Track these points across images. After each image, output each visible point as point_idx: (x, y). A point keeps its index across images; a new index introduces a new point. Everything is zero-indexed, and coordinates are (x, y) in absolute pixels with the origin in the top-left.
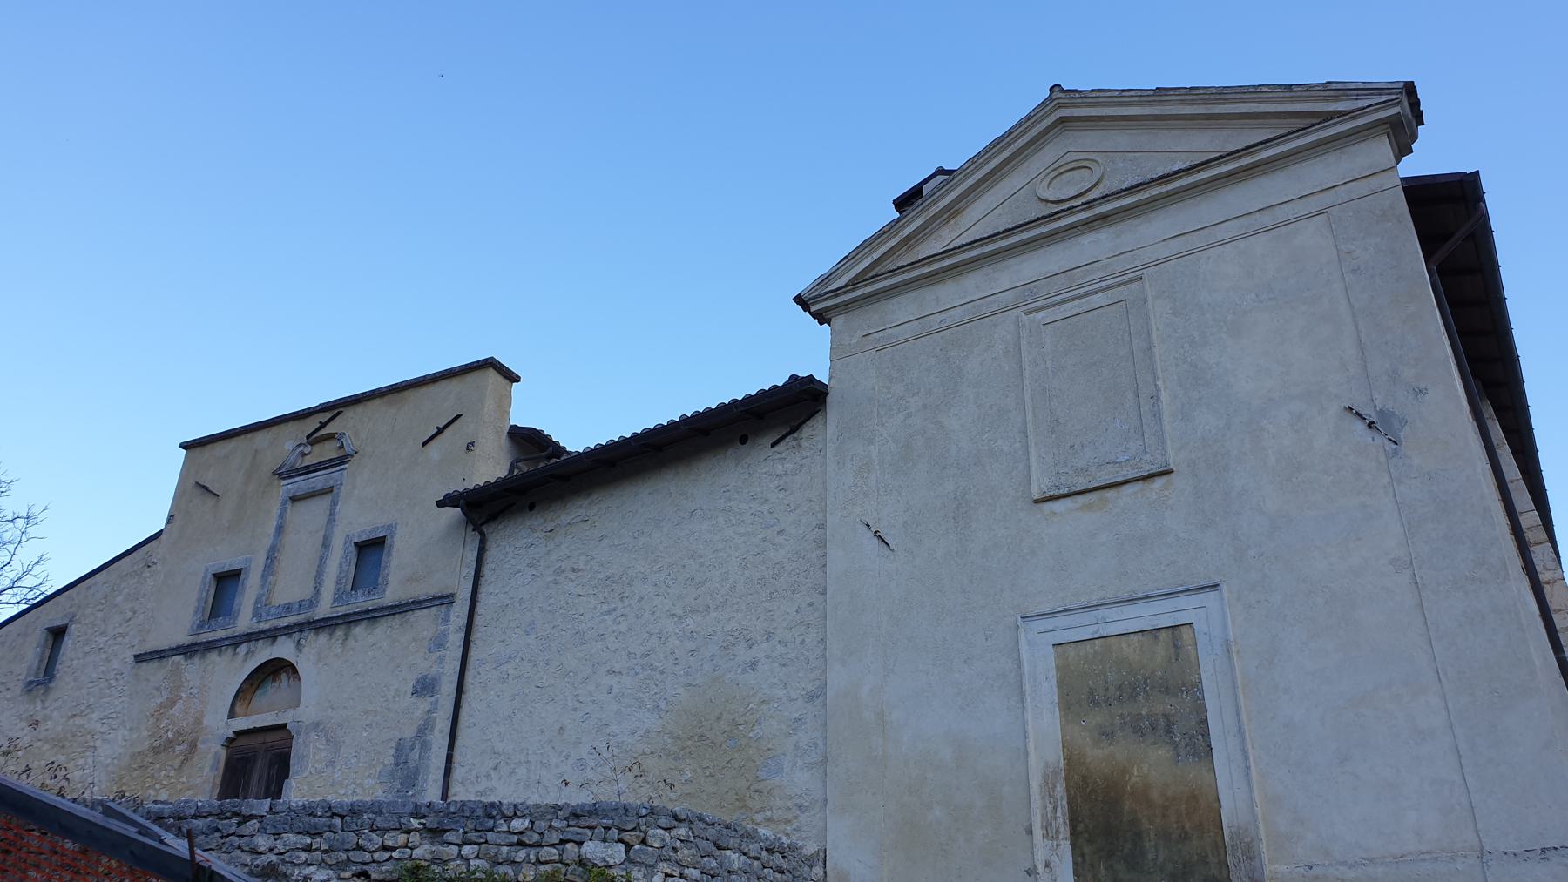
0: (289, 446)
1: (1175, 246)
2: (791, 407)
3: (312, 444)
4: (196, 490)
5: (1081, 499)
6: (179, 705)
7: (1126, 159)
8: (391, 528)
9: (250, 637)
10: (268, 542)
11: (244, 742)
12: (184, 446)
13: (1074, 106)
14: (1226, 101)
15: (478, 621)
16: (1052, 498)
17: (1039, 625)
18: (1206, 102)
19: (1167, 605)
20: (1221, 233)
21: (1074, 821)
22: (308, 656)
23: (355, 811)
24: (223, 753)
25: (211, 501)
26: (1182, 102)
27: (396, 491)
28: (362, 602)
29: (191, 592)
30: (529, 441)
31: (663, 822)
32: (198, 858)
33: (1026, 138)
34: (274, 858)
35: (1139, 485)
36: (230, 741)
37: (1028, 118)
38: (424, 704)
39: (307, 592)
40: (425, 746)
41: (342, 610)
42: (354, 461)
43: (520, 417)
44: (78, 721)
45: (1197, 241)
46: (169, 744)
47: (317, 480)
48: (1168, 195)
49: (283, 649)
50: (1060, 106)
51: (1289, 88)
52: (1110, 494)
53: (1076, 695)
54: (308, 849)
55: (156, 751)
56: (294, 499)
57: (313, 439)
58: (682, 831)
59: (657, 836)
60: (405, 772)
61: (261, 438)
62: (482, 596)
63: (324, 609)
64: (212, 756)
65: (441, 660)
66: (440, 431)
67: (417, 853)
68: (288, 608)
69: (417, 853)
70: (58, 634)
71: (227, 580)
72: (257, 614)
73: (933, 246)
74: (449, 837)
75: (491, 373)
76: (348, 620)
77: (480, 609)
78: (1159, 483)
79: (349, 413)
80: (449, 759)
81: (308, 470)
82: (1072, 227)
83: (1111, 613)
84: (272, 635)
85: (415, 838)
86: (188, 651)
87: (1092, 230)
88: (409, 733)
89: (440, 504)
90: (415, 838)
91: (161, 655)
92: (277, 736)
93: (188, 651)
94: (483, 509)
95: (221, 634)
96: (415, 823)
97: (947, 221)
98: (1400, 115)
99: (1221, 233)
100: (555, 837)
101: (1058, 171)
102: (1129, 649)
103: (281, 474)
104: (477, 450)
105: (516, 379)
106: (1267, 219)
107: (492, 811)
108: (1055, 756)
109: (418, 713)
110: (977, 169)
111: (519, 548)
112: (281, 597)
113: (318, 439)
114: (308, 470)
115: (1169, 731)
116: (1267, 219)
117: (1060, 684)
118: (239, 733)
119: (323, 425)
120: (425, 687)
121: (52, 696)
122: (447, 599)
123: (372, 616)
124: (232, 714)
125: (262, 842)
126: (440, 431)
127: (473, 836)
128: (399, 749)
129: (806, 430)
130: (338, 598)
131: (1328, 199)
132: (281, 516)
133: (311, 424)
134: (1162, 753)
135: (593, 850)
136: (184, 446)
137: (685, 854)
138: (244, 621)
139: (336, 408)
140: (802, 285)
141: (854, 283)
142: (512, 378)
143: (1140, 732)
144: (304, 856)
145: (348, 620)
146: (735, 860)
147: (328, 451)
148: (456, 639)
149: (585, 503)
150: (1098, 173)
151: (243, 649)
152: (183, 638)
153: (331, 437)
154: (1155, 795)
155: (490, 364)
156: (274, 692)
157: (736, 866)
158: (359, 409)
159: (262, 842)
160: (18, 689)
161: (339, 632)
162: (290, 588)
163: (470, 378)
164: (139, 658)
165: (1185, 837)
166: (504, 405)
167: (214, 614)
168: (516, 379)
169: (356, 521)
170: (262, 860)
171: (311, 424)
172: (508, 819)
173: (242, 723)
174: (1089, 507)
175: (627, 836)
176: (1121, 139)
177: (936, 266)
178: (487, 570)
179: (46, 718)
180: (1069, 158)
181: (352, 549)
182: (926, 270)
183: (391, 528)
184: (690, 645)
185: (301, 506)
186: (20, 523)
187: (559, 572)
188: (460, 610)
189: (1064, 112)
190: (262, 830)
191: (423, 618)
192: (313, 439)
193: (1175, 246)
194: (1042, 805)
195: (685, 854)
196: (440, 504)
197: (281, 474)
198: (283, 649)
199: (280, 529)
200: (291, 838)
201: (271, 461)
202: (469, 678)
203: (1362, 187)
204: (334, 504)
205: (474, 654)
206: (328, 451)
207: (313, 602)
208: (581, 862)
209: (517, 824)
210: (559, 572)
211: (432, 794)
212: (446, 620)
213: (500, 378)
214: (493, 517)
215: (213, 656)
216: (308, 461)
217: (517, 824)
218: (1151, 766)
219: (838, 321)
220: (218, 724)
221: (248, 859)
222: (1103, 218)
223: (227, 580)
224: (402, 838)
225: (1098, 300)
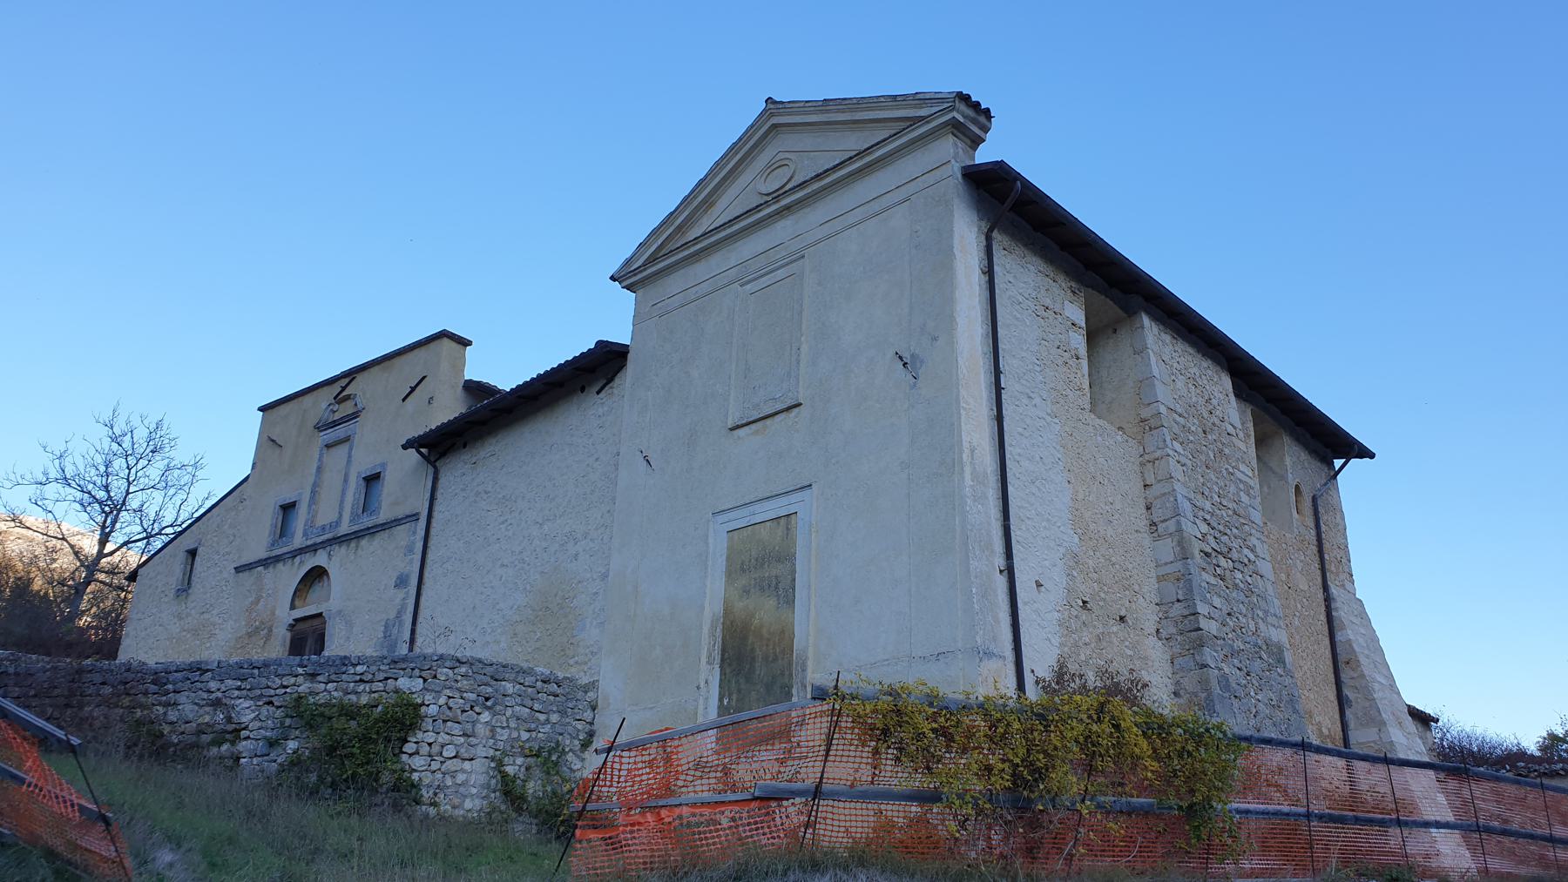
0: (324, 406)
1: (827, 229)
2: (603, 364)
3: (339, 403)
4: (269, 443)
5: (753, 426)
6: (262, 602)
7: (809, 155)
8: (384, 465)
9: (301, 551)
10: (311, 480)
11: (301, 626)
12: (261, 409)
13: (780, 115)
14: (862, 110)
15: (433, 532)
16: (738, 427)
17: (722, 518)
18: (851, 110)
19: (784, 500)
20: (851, 218)
21: (724, 651)
22: (335, 562)
23: (266, 665)
24: (289, 635)
25: (278, 451)
26: (838, 111)
27: (382, 440)
28: (367, 521)
29: (268, 517)
30: (475, 390)
31: (448, 664)
32: (1363, 786)
33: (751, 143)
34: (219, 694)
35: (783, 415)
36: (292, 626)
37: (752, 126)
38: (401, 594)
39: (334, 517)
40: (401, 624)
41: (356, 528)
42: (362, 414)
43: (473, 373)
44: (206, 616)
45: (837, 225)
46: (257, 630)
47: (340, 431)
48: (824, 189)
49: (320, 559)
50: (772, 115)
51: (894, 97)
52: (768, 422)
53: (737, 567)
54: (239, 689)
55: (249, 635)
56: (328, 446)
57: (340, 399)
58: (463, 670)
59: (443, 673)
60: (388, 638)
61: (308, 399)
62: (435, 514)
63: (344, 529)
64: (282, 635)
65: (411, 561)
66: (413, 389)
67: (301, 689)
68: (323, 528)
69: (301, 689)
70: (193, 553)
71: (288, 508)
72: (305, 534)
73: (692, 235)
74: (320, 678)
75: (446, 340)
76: (357, 536)
77: (434, 524)
78: (796, 410)
79: (360, 378)
80: (413, 632)
81: (335, 424)
82: (770, 216)
83: (757, 507)
84: (313, 549)
85: (300, 679)
86: (265, 563)
87: (783, 217)
88: (392, 615)
89: (405, 447)
90: (300, 679)
91: (249, 567)
92: (316, 622)
93: (265, 563)
94: (440, 446)
95: (285, 550)
96: (300, 670)
97: (706, 211)
98: (969, 117)
99: (851, 218)
100: (381, 676)
101: (772, 168)
102: (764, 532)
103: (321, 427)
104: (435, 403)
105: (469, 343)
106: (876, 206)
107: (345, 661)
108: (719, 608)
109: (398, 601)
110: (721, 169)
111: (459, 474)
112: (321, 520)
113: (332, 406)
114: (335, 424)
115: (777, 588)
116: (876, 206)
117: (728, 559)
118: (296, 620)
119: (344, 389)
120: (401, 582)
121: (191, 598)
122: (414, 517)
123: (371, 531)
124: (293, 607)
125: (213, 685)
126: (413, 389)
127: (333, 677)
128: (386, 626)
129: (617, 381)
130: (354, 518)
131: (912, 187)
132: (320, 460)
133: (336, 388)
134: (772, 602)
135: (403, 683)
136: (261, 409)
137: (464, 684)
138: (298, 541)
139: (351, 374)
140: (614, 266)
141: (652, 259)
142: (465, 343)
143: (762, 589)
144: (237, 693)
145: (357, 536)
146: (509, 687)
147: (347, 409)
148: (420, 545)
149: (493, 441)
150: (792, 167)
151: (298, 559)
152: (263, 555)
153: (348, 397)
154: (764, 631)
155: (444, 335)
156: (317, 591)
157: (510, 691)
158: (365, 374)
159: (213, 685)
160: (172, 595)
161: (353, 544)
162: (326, 515)
163: (432, 345)
164: (238, 570)
165: (775, 659)
166: (460, 364)
167: (281, 536)
168: (469, 343)
169: (364, 463)
170: (213, 696)
171: (336, 388)
172: (354, 665)
173: (298, 613)
174: (756, 432)
175: (424, 674)
176: (806, 141)
177: (692, 250)
178: (438, 495)
179: (188, 615)
180: (782, 156)
181: (363, 483)
182: (686, 253)
183: (384, 465)
184: (544, 544)
185: (333, 450)
186: (190, 469)
187: (478, 494)
188: (422, 523)
189: (776, 120)
190: (213, 678)
191: (401, 531)
192: (340, 399)
193: (827, 229)
194: (707, 643)
195: (464, 684)
196: (405, 447)
197: (321, 427)
198: (320, 559)
199: (319, 469)
200: (230, 682)
201: (313, 420)
202: (426, 574)
203: (930, 179)
204: (351, 449)
205: (430, 556)
206: (347, 409)
207: (338, 523)
208: (397, 691)
209: (360, 669)
210: (478, 494)
211: (403, 650)
212: (414, 533)
213: (453, 345)
214: (443, 455)
215: (280, 565)
216: (337, 416)
217: (360, 669)
218: (764, 611)
219: (640, 292)
220: (285, 615)
221: (205, 695)
222: (788, 208)
223: (288, 508)
224: (292, 680)
225: (780, 274)
